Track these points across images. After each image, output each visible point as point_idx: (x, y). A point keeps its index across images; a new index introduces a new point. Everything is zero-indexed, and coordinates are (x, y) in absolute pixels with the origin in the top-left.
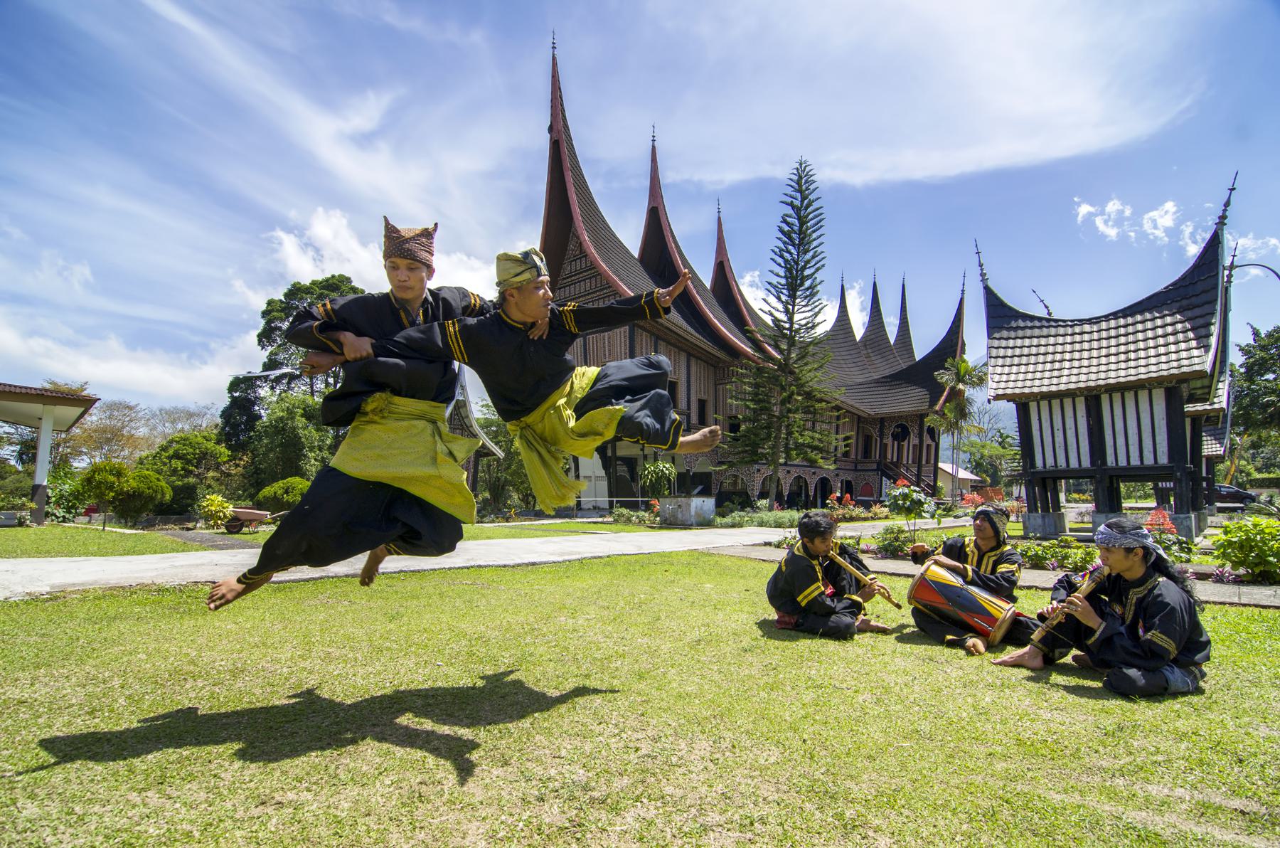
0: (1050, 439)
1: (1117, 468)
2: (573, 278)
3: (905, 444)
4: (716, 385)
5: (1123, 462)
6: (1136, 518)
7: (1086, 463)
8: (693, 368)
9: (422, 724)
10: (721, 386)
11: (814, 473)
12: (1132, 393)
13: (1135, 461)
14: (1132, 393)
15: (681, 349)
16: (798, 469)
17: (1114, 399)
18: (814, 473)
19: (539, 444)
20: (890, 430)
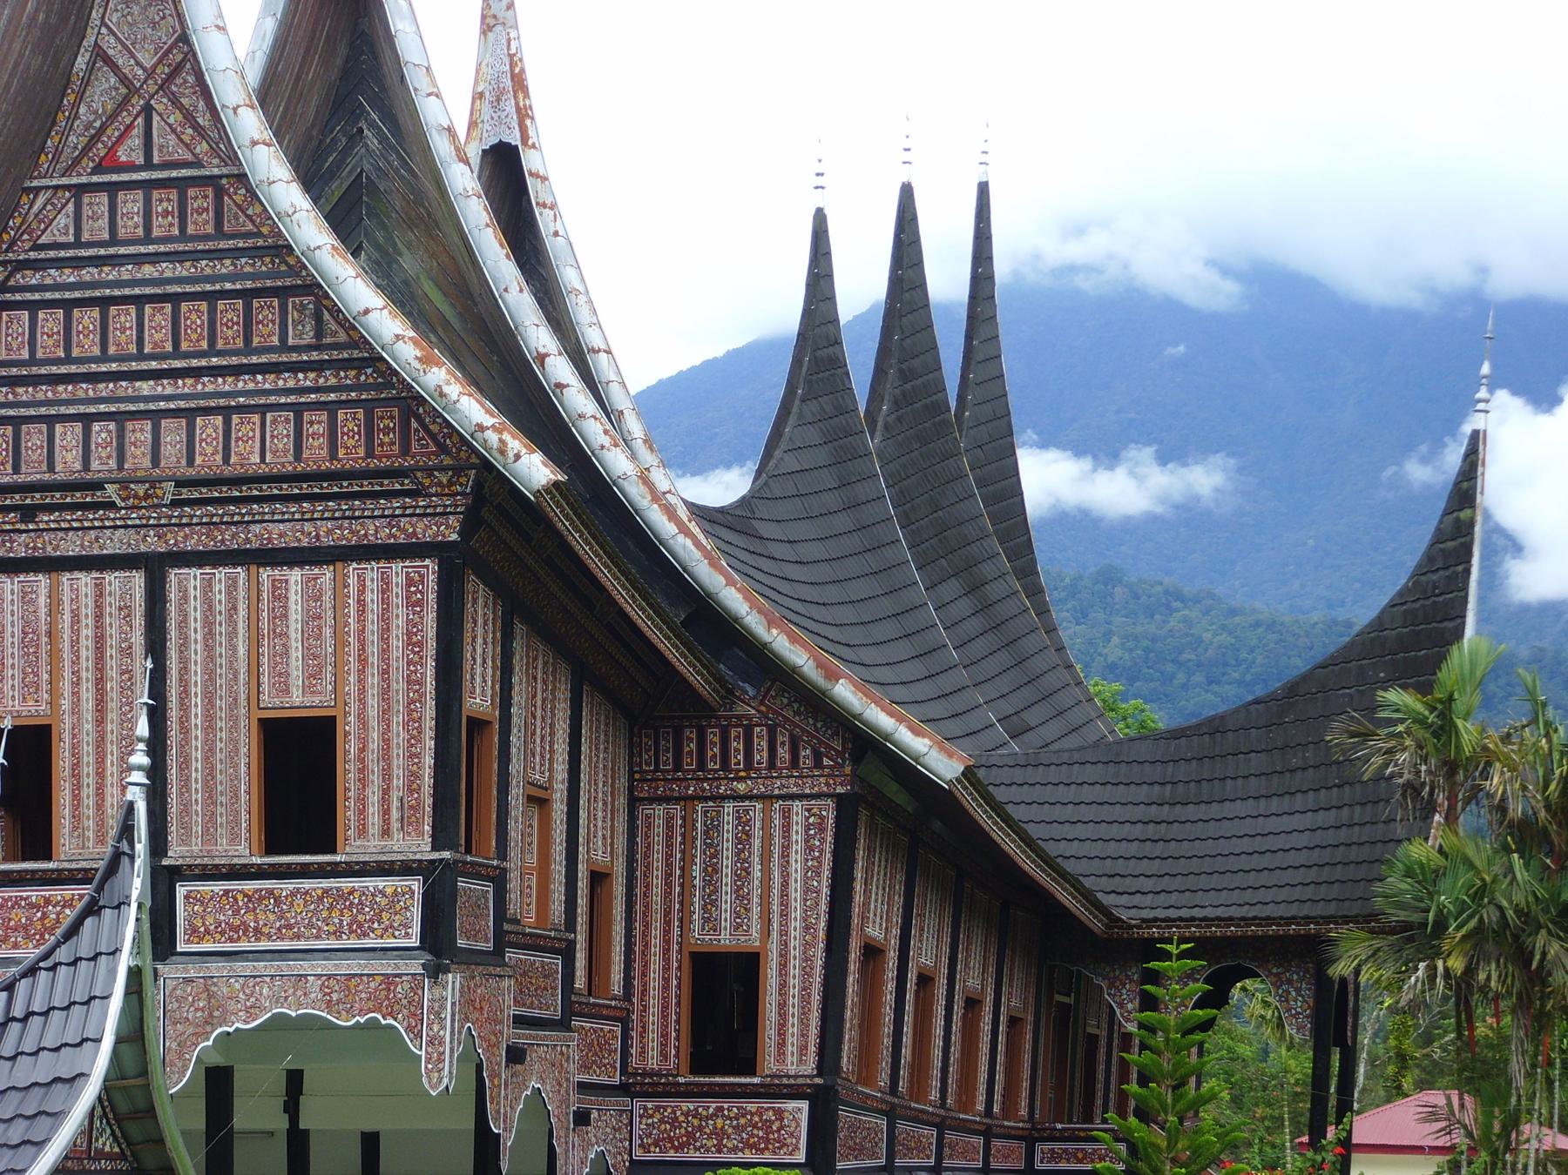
4: (633, 802)
10: (659, 810)
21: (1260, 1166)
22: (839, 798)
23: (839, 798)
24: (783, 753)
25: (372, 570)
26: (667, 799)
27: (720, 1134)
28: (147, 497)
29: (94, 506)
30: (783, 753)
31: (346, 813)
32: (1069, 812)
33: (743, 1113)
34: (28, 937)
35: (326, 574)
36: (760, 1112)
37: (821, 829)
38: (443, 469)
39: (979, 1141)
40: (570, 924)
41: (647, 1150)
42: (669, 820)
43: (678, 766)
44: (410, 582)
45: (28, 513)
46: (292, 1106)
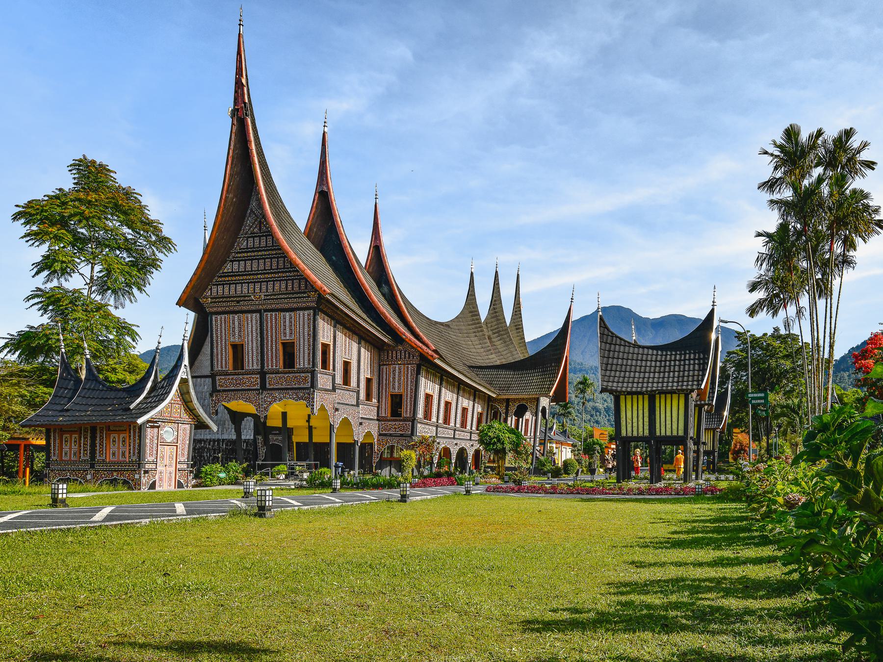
0: (676, 419)
1: (660, 437)
2: (237, 278)
3: (521, 419)
4: (380, 366)
5: (663, 434)
6: (585, 467)
7: (647, 433)
8: (363, 350)
9: (185, 365)
10: (385, 367)
11: (456, 444)
12: (670, 395)
13: (635, 434)
14: (670, 395)
15: (354, 333)
16: (445, 440)
17: (639, 399)
18: (456, 444)
19: (28, 513)
20: (513, 408)
21: (596, 452)
22: (417, 364)
23: (417, 364)
24: (407, 356)
25: (301, 313)
26: (386, 365)
27: (395, 428)
28: (259, 298)
29: (250, 300)
30: (407, 356)
31: (297, 360)
32: (635, 424)
33: (400, 424)
34: (240, 385)
35: (292, 314)
36: (403, 424)
37: (414, 370)
38: (313, 292)
39: (434, 428)
40: (358, 386)
41: (382, 431)
42: (386, 369)
43: (388, 358)
44: (308, 315)
45: (238, 302)
46: (308, 421)
